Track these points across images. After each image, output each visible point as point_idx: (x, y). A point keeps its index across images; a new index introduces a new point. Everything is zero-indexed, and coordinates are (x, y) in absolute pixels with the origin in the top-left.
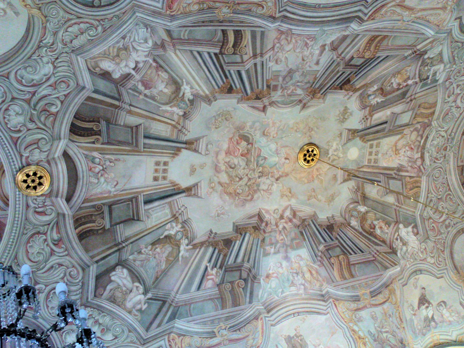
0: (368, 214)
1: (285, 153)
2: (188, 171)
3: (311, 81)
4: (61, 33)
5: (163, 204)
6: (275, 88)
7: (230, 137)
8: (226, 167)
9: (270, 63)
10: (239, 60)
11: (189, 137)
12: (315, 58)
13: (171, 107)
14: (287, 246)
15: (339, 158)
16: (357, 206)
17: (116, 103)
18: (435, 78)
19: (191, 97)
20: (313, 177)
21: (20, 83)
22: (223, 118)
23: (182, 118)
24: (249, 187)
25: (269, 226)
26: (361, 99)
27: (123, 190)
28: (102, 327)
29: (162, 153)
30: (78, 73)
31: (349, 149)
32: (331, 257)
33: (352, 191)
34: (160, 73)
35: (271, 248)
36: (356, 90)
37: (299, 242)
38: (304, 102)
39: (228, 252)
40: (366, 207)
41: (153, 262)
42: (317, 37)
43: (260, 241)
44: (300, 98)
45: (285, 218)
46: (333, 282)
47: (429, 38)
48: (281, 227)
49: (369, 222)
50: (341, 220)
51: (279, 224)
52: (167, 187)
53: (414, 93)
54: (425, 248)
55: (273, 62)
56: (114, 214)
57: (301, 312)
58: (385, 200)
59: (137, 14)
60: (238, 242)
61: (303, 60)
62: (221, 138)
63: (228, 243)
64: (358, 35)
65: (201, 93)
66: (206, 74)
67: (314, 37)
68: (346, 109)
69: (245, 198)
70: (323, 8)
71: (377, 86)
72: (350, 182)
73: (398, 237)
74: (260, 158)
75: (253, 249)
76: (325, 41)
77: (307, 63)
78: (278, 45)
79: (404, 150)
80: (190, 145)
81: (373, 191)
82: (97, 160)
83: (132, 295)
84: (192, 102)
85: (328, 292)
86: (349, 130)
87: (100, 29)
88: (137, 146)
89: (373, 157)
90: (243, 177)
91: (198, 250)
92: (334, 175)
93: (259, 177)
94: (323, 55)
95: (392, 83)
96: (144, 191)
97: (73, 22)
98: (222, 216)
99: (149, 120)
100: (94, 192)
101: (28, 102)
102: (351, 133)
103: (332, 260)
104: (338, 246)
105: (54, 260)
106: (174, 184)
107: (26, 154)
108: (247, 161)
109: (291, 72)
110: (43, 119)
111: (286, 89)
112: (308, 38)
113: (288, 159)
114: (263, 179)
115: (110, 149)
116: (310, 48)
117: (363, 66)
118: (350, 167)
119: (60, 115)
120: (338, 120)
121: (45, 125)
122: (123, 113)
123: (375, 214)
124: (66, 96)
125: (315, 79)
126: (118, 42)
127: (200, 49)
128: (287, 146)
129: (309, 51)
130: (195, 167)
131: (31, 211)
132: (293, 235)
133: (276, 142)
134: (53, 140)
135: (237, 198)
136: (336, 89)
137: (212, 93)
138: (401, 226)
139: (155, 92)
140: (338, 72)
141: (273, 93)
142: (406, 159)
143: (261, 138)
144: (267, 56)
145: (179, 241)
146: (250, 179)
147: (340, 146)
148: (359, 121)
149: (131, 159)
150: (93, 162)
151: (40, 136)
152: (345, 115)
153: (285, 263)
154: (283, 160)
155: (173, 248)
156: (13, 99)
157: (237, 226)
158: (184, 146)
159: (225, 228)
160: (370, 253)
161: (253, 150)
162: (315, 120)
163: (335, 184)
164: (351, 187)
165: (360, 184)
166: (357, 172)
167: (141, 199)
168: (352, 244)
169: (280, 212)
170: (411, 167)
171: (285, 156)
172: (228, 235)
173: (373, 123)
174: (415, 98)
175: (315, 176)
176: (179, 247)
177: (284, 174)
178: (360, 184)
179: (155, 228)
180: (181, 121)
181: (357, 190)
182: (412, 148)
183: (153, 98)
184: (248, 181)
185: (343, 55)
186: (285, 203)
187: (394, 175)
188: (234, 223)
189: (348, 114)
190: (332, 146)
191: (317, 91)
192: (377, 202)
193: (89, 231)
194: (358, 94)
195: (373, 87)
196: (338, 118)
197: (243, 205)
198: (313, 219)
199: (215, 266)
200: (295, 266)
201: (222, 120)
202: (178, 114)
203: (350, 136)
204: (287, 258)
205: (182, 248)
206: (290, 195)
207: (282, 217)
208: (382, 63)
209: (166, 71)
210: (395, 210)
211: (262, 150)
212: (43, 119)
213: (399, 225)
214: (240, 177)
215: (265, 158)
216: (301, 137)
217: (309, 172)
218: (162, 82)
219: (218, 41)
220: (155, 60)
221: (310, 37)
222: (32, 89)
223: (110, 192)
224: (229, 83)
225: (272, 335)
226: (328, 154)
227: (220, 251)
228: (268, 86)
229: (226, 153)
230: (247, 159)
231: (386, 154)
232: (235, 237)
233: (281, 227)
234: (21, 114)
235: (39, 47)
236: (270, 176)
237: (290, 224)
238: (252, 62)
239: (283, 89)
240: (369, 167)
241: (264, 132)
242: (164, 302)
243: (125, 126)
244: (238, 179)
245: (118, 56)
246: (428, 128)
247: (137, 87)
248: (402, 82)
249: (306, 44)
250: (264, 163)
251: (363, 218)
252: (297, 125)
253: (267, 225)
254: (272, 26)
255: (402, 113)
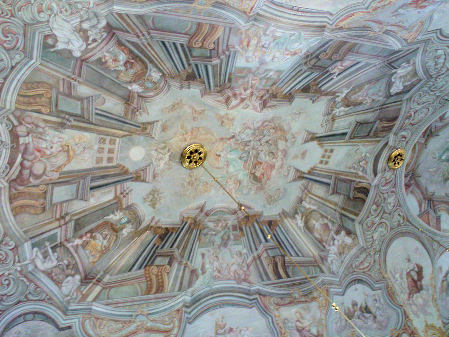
0: (129, 80)
1: (219, 162)
2: (307, 155)
3: (203, 236)
4: (372, 261)
5: (335, 131)
6: (234, 228)
7: (268, 181)
8: (277, 154)
9: (246, 252)
10: (269, 251)
11: (301, 183)
12: (207, 260)
13: (310, 208)
14: (254, 73)
15: (156, 150)
16: (142, 92)
17: (343, 212)
18: (40, 249)
19: (296, 216)
20: (192, 133)
21: (386, 225)
22: (273, 198)
23: (303, 199)
24: (263, 133)
25: (260, 95)
26: (138, 217)
27: (355, 145)
28: (437, 60)
29: (321, 171)
30: (362, 234)
31: (143, 159)
32: (211, 50)
33: (144, 110)
34: (320, 237)
35: (271, 76)
36: (148, 228)
37: (238, 73)
38: (203, 214)
39: (311, 82)
40: (130, 88)
41: (371, 91)
42: (212, 280)
43: (277, 84)
44: (208, 218)
45: (240, 99)
46: (231, 29)
47: (94, 300)
48: (248, 92)
49: (131, 72)
50: (171, 82)
51: (249, 95)
52: (327, 143)
53: (64, 227)
54: (39, 12)
55: (244, 253)
56: (369, 129)
57: (290, 9)
58: (93, 90)
59: (338, 280)
60: (297, 88)
61: (217, 257)
62: (277, 180)
63: (306, 90)
64: (180, 290)
65: (289, 219)
66: (289, 237)
67: (214, 279)
68: (153, 205)
69: (270, 124)
70: (217, 306)
71: (123, 235)
72: (144, 121)
73: (90, 42)
74: (245, 159)
75: (289, 79)
76: (205, 278)
77: (213, 254)
78: (245, 269)
79: (54, 150)
80: (300, 176)
81: (113, 105)
82: (361, 169)
83: (402, 75)
84: (296, 213)
85: (247, 22)
86: (144, 181)
87: (354, 266)
88: (336, 178)
89: (107, 146)
90: (265, 144)
91: (333, 90)
92: (165, 132)
93: (250, 141)
94: (201, 264)
95: (104, 238)
96: (344, 142)
97: (367, 269)
98: (297, 112)
99: (325, 198)
100: (372, 147)
101: (385, 212)
102: (142, 178)
103: (212, 46)
104: (194, 57)
105: (418, 107)
106: (321, 145)
107: (393, 176)
108: (257, 157)
109: (224, 243)
110: (380, 200)
111: (224, 227)
112: (220, 278)
113: (217, 155)
114: (248, 139)
115: (352, 176)
116: (215, 269)
117: (152, 256)
118: (142, 138)
119: (372, 202)
120: (161, 193)
121: (380, 196)
122: (340, 204)
123: (117, 78)
124: (368, 217)
125: (199, 239)
126: (345, 258)
127: (298, 259)
128: (217, 168)
129: (215, 266)
130: (301, 157)
131: (407, 140)
132: (241, 81)
133: (228, 173)
134: (378, 185)
135: (276, 125)
136: (173, 229)
137: (282, 220)
138: (77, 54)
139: (321, 221)
140: (178, 247)
141: (236, 222)
142: (48, 138)
143: (242, 178)
144: (250, 258)
145: (342, 101)
146: (260, 140)
147: (154, 163)
148: (133, 192)
149: (341, 168)
150: (363, 168)
151: (384, 188)
152: (153, 199)
153: (268, 59)
154: (222, 155)
155: (350, 97)
156: (390, 214)
157: (290, 101)
158: (305, 176)
159: (301, 101)
160: (152, 38)
161: (250, 168)
162: (187, 193)
163: (166, 122)
164: (145, 115)
165: (129, 117)
166: (132, 130)
167: (347, 137)
168: (171, 51)
169: (242, 105)
170: (37, 126)
171: (220, 158)
172: (302, 95)
173: (112, 188)
174: (58, 220)
175: (190, 133)
176: (345, 97)
177: (225, 140)
178: (129, 117)
179: (351, 114)
180: (304, 196)
181: (136, 110)
182: (39, 151)
183: (322, 216)
184: (261, 139)
185: (182, 267)
186: (233, 113)
187: (71, 119)
188: (291, 104)
189: (149, 200)
190: (165, 164)
191: (193, 226)
192: (109, 91)
193: (391, 121)
194: (144, 225)
195: (128, 233)
196: (160, 195)
197: (274, 118)
198: (208, 91)
199: (331, 74)
200: (259, 54)
201: (274, 196)
202: (306, 202)
203: (142, 174)
204: (262, 63)
205: (344, 95)
206: (224, 119)
207: (243, 100)
208: (132, 262)
209: (316, 238)
210: (79, 75)
211: (242, 166)
212: (380, 200)
213: (81, 57)
214: (268, 144)
215: (240, 158)
216: (201, 177)
217: (195, 138)
218: (317, 229)
219: (289, 267)
220: (325, 247)
221: (219, 279)
222: (383, 220)
223: (363, 146)
224: (272, 231)
225: (340, 7)
226: (170, 156)
227: (317, 85)
228: (241, 229)
229: (274, 166)
230: (257, 160)
231: (84, 148)
232: (297, 93)
233: (248, 92)
234: (388, 203)
235: (380, 251)
236: (240, 141)
237: (237, 92)
238: (259, 251)
239: (226, 227)
240: (114, 135)
241: (240, 185)
242: (389, 64)
243: (339, 194)
244: (270, 142)
245: (344, 248)
246: (14, 177)
247: (332, 225)
248: (90, 241)
249: (219, 272)
250: (242, 154)
251: (138, 78)
252: (207, 189)
253: (262, 97)
254: (256, 287)
255: (71, 200)
